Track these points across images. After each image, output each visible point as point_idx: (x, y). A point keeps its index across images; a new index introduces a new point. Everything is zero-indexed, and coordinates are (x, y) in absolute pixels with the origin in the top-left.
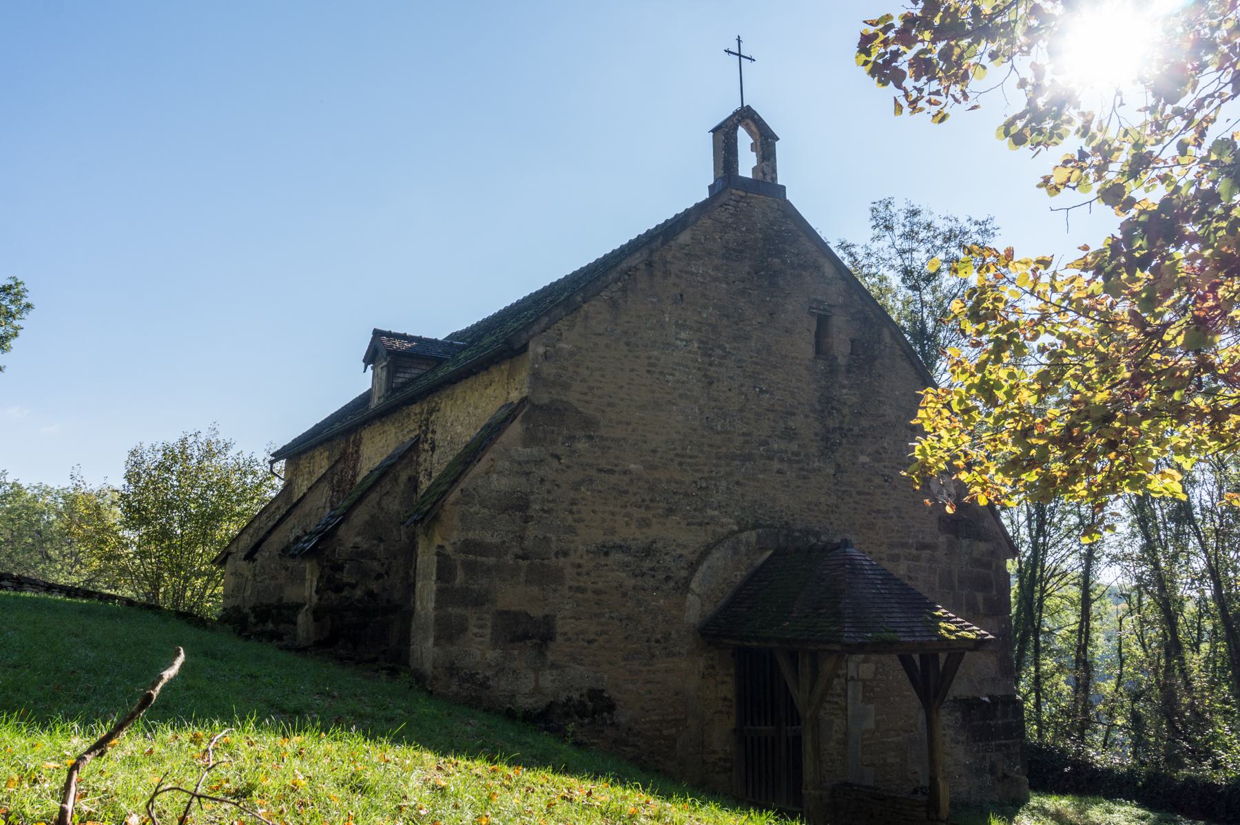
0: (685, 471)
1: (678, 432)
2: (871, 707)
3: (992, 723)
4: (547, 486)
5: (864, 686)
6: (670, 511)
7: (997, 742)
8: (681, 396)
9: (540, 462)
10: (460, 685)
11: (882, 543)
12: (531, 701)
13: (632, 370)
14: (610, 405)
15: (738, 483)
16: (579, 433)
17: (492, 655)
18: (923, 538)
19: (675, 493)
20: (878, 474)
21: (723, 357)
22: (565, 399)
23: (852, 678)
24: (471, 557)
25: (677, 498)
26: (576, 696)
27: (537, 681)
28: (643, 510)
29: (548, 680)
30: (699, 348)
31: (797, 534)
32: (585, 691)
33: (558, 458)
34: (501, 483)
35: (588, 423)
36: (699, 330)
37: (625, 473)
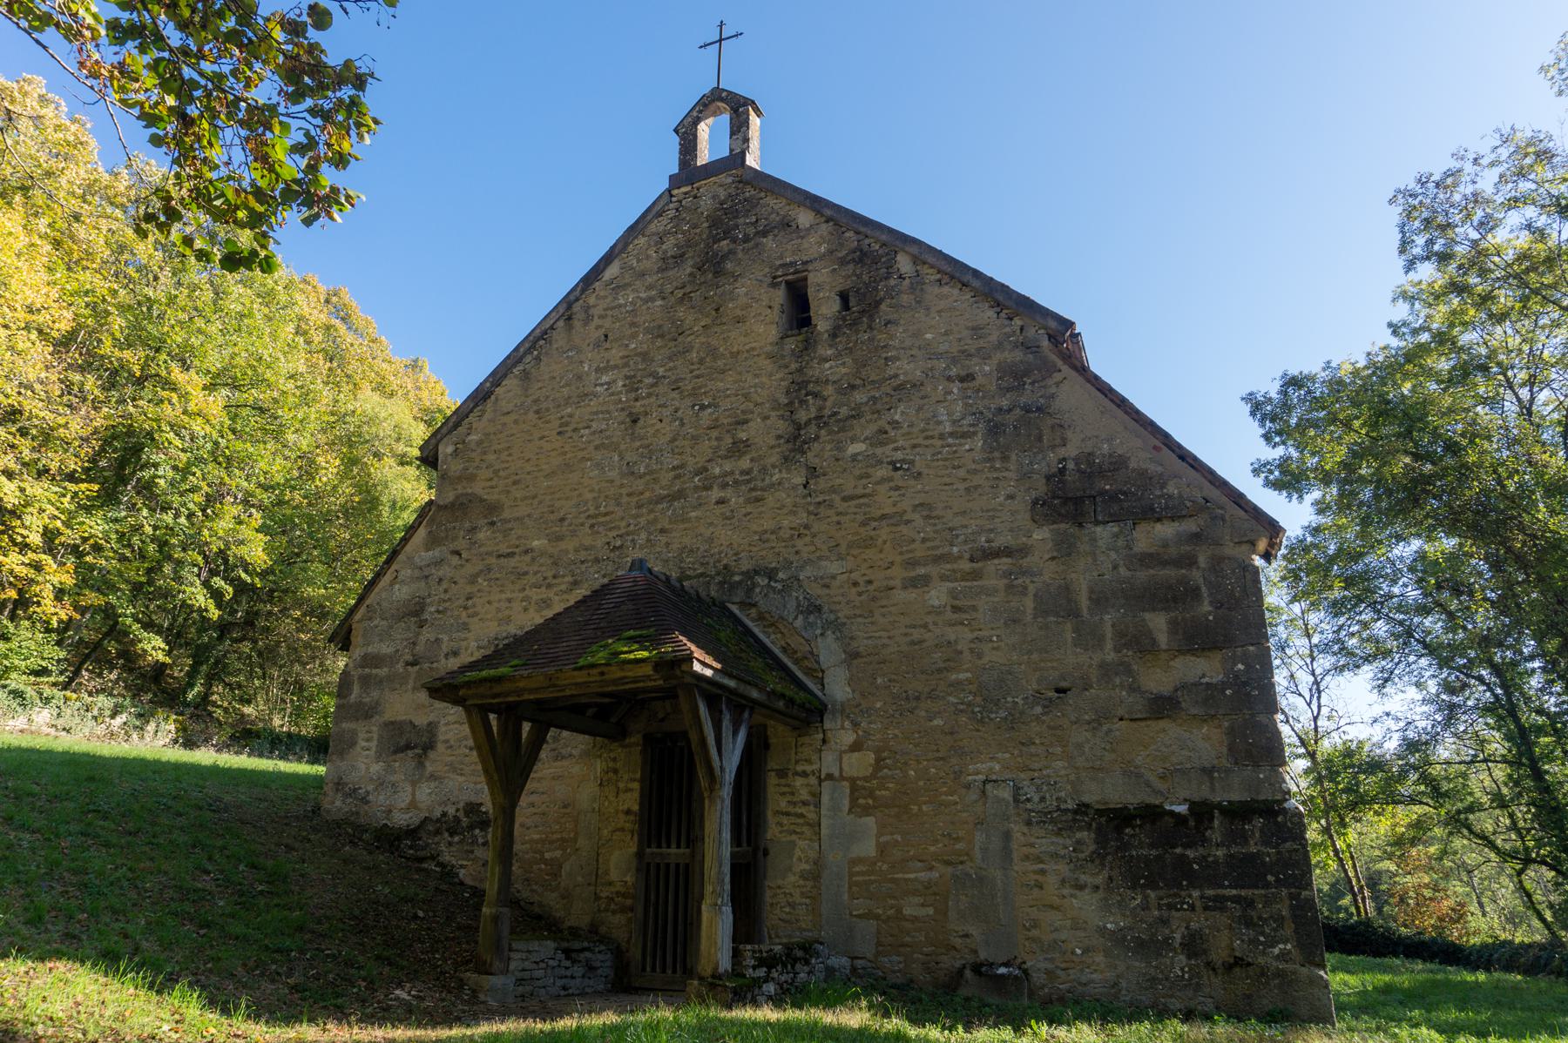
0: (598, 533)
1: (592, 491)
3: (1190, 853)
4: (445, 585)
7: (1210, 892)
8: (597, 448)
9: (439, 563)
12: (407, 816)
13: (541, 438)
14: (515, 483)
18: (988, 541)
21: (652, 386)
23: (830, 777)
26: (451, 811)
27: (413, 795)
28: (543, 589)
29: (426, 794)
30: (624, 386)
32: (461, 805)
33: (458, 553)
35: (492, 509)
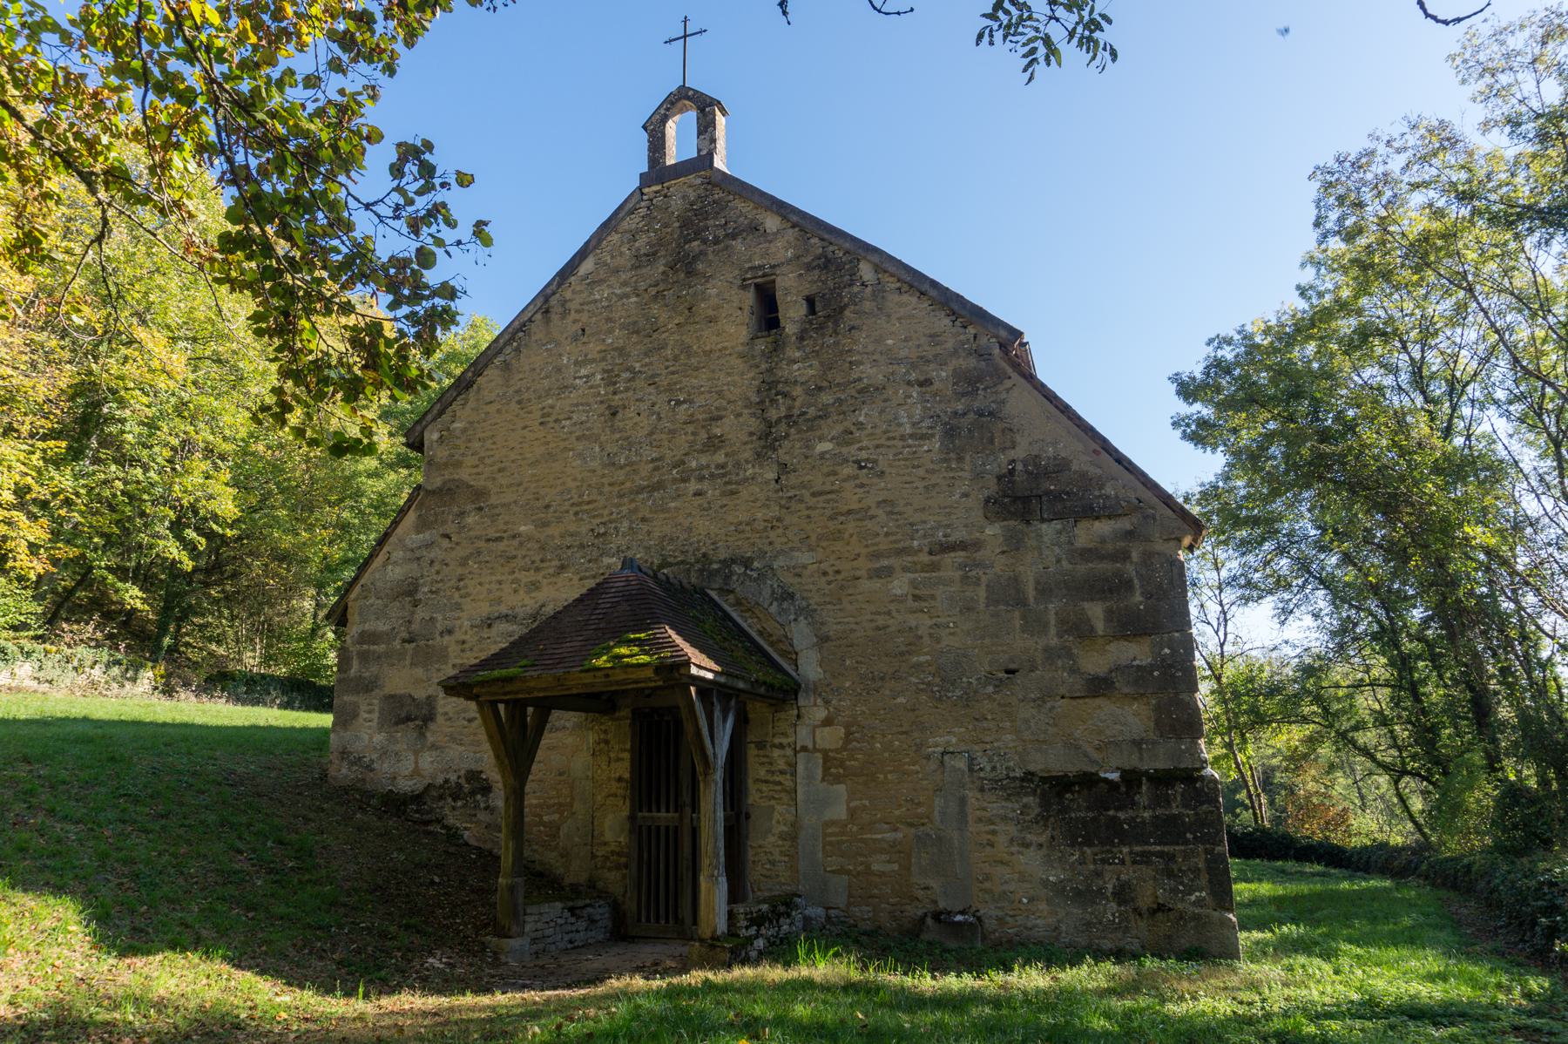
0: (582, 519)
1: (575, 480)
2: (842, 788)
3: (1122, 815)
4: (437, 567)
5: (826, 759)
6: (562, 568)
7: (1138, 849)
8: (578, 439)
9: (429, 545)
10: (349, 768)
11: (859, 555)
12: (411, 783)
13: (525, 428)
14: (500, 470)
15: (644, 520)
16: (469, 507)
17: (379, 738)
19: (568, 547)
20: (848, 461)
22: (457, 477)
23: (804, 749)
24: (365, 647)
25: (569, 552)
26: (453, 778)
27: (416, 763)
29: (427, 761)
30: (602, 379)
31: (715, 566)
32: (462, 773)
33: (448, 537)
34: (395, 573)
35: (479, 495)
36: (604, 359)
37: (514, 537)
